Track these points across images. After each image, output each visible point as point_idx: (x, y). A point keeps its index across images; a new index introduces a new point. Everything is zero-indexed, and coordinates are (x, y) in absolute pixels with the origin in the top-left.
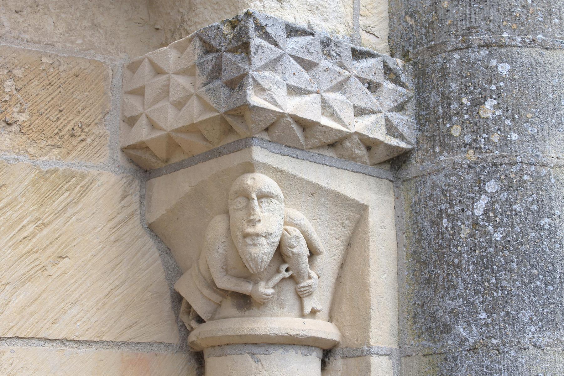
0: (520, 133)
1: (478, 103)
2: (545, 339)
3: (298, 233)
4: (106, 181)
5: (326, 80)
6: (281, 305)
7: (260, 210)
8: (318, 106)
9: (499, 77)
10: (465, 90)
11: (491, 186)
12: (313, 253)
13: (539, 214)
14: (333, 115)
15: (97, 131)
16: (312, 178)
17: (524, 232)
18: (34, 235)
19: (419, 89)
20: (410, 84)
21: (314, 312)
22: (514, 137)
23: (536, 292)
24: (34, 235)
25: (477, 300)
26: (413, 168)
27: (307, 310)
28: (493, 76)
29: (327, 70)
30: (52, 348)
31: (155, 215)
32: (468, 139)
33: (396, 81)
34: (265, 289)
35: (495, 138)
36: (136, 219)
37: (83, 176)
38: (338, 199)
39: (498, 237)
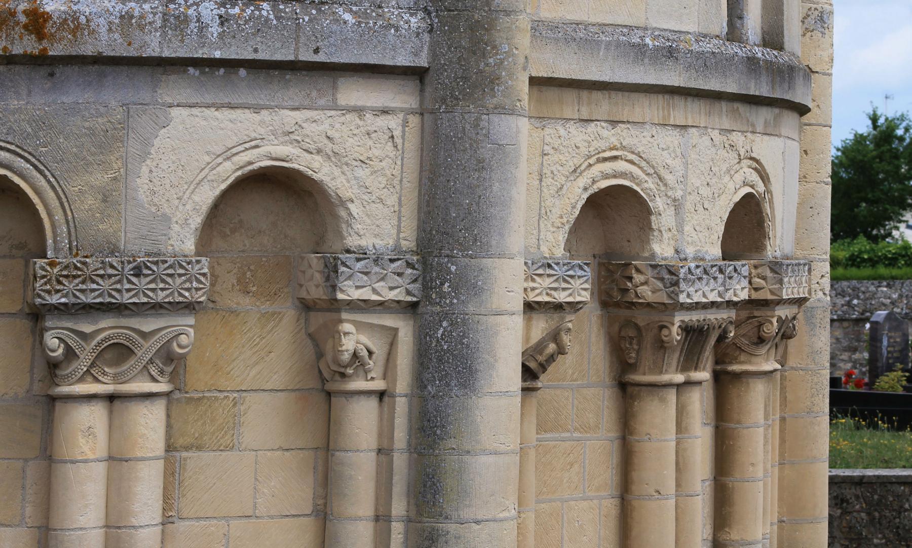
0: (458, 299)
1: (442, 284)
2: (460, 393)
3: (362, 347)
4: (290, 314)
5: (374, 278)
6: (358, 377)
7: (344, 340)
8: (371, 292)
9: (451, 272)
10: (437, 277)
11: (445, 324)
12: (370, 353)
13: (464, 337)
14: (378, 294)
15: (286, 290)
16: (370, 321)
17: (456, 345)
18: (259, 343)
19: (424, 271)
20: (420, 268)
21: (372, 379)
22: (455, 301)
23: (459, 372)
24: (259, 343)
25: (436, 375)
26: (421, 309)
27: (369, 378)
28: (449, 272)
29: (376, 273)
30: (266, 394)
31: (312, 330)
32: (438, 300)
33: (413, 268)
34: (350, 371)
35: (448, 301)
36: (303, 330)
37: (280, 313)
38: (383, 327)
39: (446, 347)
